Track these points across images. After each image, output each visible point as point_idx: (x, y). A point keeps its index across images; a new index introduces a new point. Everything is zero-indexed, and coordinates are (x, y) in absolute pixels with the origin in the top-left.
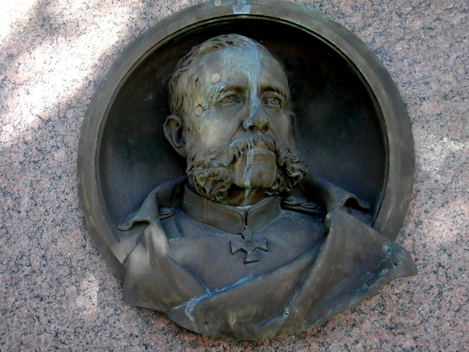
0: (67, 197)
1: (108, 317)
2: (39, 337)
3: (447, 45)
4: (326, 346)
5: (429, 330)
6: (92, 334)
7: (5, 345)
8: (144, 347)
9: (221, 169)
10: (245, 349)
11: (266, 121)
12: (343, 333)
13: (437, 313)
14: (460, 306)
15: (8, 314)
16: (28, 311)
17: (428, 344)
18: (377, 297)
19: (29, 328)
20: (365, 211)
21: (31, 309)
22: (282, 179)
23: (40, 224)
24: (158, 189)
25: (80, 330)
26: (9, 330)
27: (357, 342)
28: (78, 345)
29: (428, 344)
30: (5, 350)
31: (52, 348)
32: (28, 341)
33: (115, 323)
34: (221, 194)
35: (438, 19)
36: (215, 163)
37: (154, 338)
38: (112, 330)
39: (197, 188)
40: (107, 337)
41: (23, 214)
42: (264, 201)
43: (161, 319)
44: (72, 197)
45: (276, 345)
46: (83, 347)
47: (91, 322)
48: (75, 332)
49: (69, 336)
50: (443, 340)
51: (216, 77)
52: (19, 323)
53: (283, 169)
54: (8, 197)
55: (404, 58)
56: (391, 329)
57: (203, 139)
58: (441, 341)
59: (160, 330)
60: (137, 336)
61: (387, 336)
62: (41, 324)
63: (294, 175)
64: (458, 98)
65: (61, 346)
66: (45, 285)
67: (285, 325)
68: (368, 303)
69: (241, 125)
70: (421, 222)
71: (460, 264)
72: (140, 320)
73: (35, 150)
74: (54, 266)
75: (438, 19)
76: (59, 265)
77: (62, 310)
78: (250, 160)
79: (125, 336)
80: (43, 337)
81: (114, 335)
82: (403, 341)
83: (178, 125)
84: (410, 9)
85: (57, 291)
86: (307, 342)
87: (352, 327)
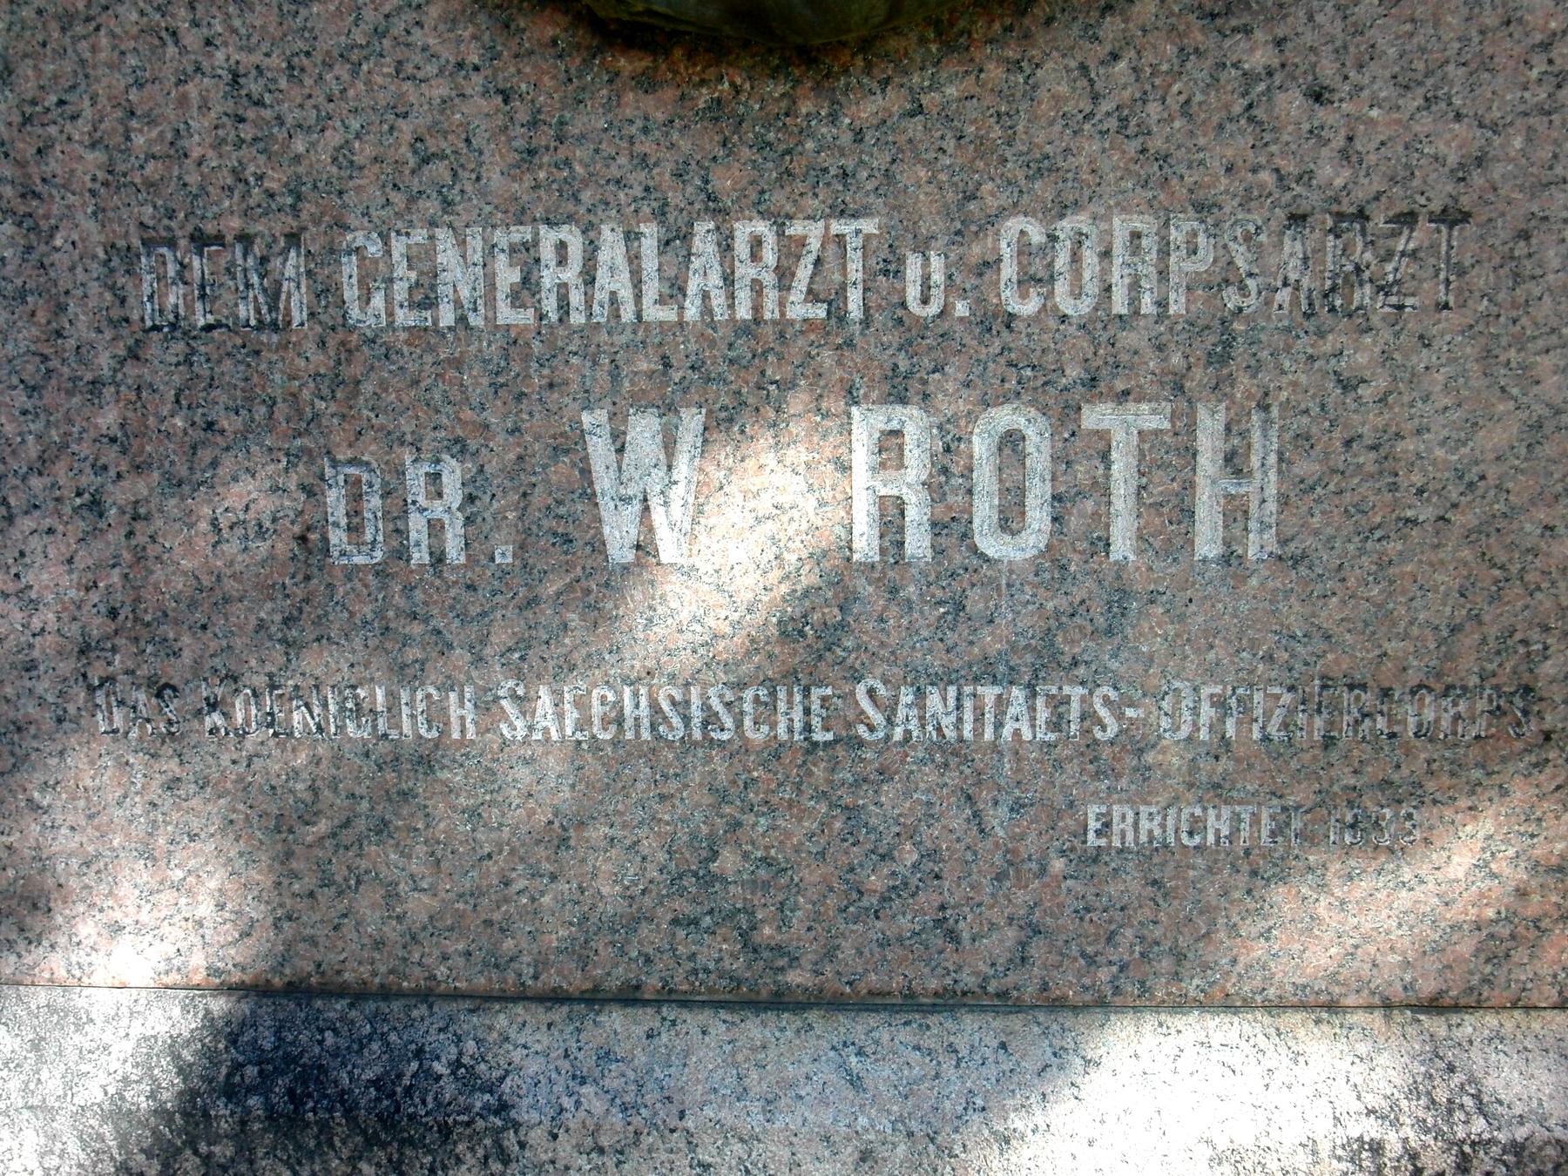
1: (387, 16)
2: (181, 89)
4: (1028, 72)
5: (1319, 18)
6: (342, 70)
7: (80, 121)
8: (500, 99)
10: (793, 88)
12: (1076, 30)
15: (79, 29)
16: (142, 13)
17: (1313, 59)
19: (148, 67)
21: (149, 9)
25: (305, 61)
26: (87, 76)
27: (1115, 57)
28: (301, 106)
29: (1313, 59)
30: (82, 133)
31: (225, 119)
32: (151, 104)
33: (408, 32)
37: (528, 70)
38: (400, 53)
40: (389, 75)
43: (547, 12)
45: (884, 71)
46: (318, 110)
47: (338, 34)
48: (291, 67)
49: (274, 81)
50: (1357, 46)
52: (116, 54)
56: (1213, 16)
58: (1352, 49)
59: (546, 45)
60: (476, 68)
61: (1200, 37)
62: (184, 50)
65: (251, 114)
72: (482, 18)
79: (441, 71)
80: (192, 89)
81: (409, 69)
82: (1244, 52)
86: (972, 60)
87: (1103, 16)
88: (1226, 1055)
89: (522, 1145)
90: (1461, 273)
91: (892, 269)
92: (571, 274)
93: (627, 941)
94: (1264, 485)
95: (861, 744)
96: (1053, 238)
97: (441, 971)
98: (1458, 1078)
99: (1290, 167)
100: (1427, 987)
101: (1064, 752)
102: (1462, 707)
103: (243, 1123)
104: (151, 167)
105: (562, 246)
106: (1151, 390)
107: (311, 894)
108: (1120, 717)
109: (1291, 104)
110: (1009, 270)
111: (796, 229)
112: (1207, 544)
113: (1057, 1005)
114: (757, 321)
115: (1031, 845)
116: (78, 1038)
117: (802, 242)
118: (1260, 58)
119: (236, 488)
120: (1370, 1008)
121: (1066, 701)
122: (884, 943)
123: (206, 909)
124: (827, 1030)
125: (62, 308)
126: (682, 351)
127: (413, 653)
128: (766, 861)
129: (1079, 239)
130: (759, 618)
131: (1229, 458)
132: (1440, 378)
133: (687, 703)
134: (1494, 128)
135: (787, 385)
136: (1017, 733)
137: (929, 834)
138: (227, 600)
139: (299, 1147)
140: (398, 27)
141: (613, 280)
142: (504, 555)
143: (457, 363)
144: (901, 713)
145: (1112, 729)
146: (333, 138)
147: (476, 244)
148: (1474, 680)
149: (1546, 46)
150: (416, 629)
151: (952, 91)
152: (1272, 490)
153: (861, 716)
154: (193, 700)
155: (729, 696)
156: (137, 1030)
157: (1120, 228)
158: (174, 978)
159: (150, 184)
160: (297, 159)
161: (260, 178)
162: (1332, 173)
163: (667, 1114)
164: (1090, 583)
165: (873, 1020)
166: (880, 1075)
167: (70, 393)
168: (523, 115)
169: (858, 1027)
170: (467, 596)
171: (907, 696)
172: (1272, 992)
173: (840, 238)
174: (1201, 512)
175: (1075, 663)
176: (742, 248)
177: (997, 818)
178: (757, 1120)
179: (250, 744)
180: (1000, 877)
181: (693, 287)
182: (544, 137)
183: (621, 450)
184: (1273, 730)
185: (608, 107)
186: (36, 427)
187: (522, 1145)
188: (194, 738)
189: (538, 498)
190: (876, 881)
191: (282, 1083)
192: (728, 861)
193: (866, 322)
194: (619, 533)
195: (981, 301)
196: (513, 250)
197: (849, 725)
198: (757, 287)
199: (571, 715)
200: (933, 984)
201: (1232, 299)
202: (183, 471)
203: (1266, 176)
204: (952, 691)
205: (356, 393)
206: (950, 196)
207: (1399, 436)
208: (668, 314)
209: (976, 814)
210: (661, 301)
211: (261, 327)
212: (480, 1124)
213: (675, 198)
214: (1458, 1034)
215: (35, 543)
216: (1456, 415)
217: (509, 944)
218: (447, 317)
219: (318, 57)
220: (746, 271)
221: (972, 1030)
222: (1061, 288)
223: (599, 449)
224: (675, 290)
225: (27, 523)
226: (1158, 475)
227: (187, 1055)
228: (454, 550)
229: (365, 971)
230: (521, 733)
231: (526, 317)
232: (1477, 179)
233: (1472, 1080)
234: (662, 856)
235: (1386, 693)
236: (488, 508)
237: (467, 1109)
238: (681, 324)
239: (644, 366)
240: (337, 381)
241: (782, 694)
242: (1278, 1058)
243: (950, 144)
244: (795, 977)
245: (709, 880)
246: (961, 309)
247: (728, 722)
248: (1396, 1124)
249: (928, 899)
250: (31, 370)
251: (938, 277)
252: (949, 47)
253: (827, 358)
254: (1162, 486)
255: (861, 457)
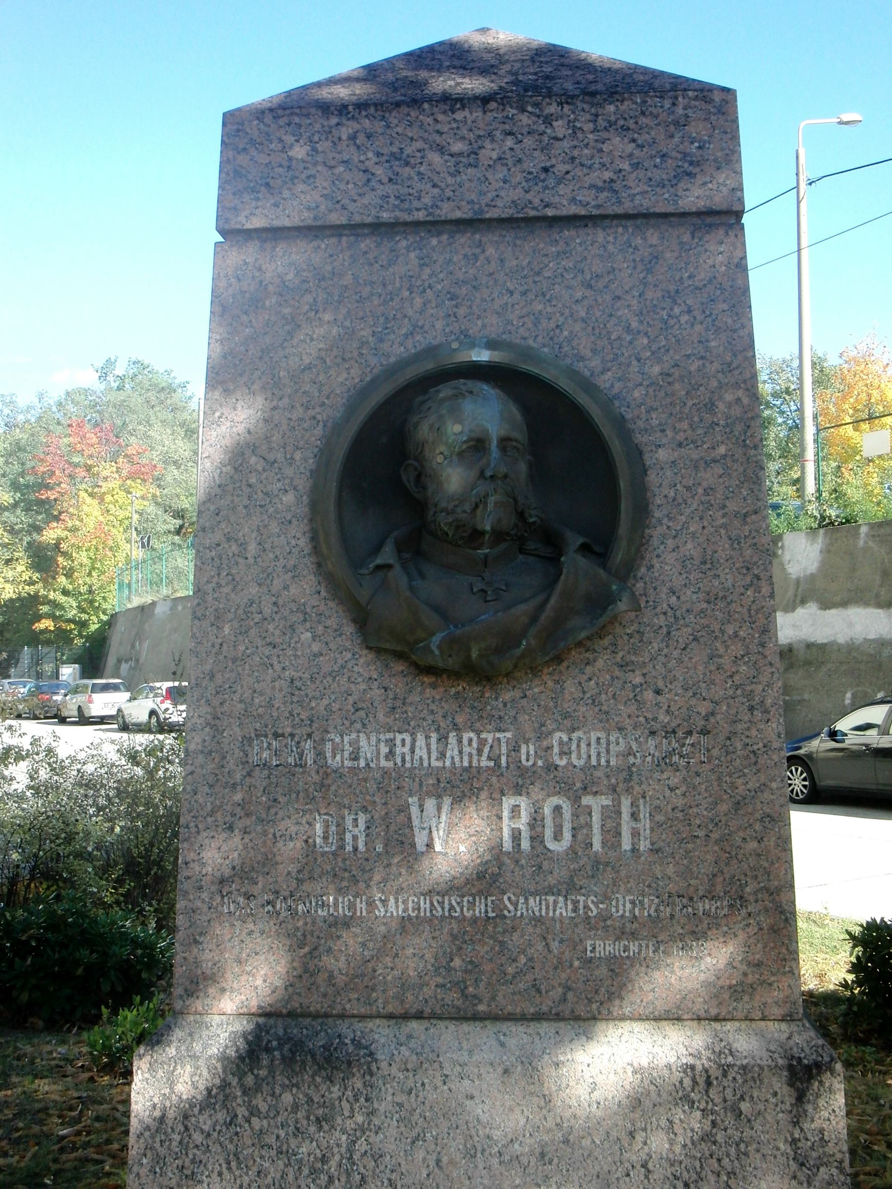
0: (299, 542)
3: (683, 393)
6: (330, 679)
9: (465, 515)
11: (505, 470)
12: (577, 670)
13: (665, 651)
14: (687, 645)
15: (239, 663)
18: (610, 637)
20: (599, 555)
22: (520, 524)
23: (270, 570)
24: (395, 533)
27: (590, 679)
34: (462, 538)
35: (676, 365)
36: (459, 510)
38: (350, 674)
39: (439, 533)
41: (251, 561)
42: (503, 546)
44: (303, 542)
51: (457, 428)
53: (521, 515)
54: (232, 543)
55: (642, 404)
57: (446, 485)
62: (275, 671)
63: (532, 520)
64: (692, 446)
65: (297, 693)
66: (277, 632)
67: (523, 656)
68: (601, 642)
69: (482, 474)
70: (652, 566)
71: (688, 606)
72: (378, 663)
73: (260, 493)
74: (286, 613)
75: (676, 365)
76: (292, 612)
77: (295, 656)
78: (490, 506)
80: (277, 684)
83: (416, 469)
84: (649, 354)
85: (291, 638)
88: (639, 1036)
89: (378, 1068)
90: (708, 751)
91: (516, 749)
92: (406, 750)
93: (419, 993)
94: (645, 824)
95: (505, 917)
96: (570, 739)
97: (348, 1007)
98: (723, 1044)
99: (649, 716)
100: (714, 1012)
101: (577, 920)
102: (719, 904)
103: (272, 1061)
104: (260, 710)
105: (403, 740)
106: (605, 791)
107: (300, 976)
108: (597, 907)
109: (649, 695)
110: (556, 750)
111: (484, 735)
112: (626, 845)
113: (578, 1018)
114: (470, 767)
115: (567, 956)
116: (207, 1032)
117: (486, 740)
118: (638, 680)
119: (283, 823)
120: (692, 1020)
121: (578, 901)
122: (514, 994)
123: (259, 982)
124: (491, 1028)
125: (225, 758)
126: (445, 776)
127: (345, 883)
128: (471, 962)
129: (579, 740)
130: (469, 871)
131: (633, 815)
132: (703, 787)
133: (443, 902)
134: (716, 703)
135: (480, 789)
136: (561, 914)
137: (530, 952)
138: (277, 863)
139: (293, 1071)
140: (349, 665)
141: (421, 751)
142: (379, 848)
143: (365, 780)
144: (520, 906)
145: (595, 912)
146: (325, 702)
147: (373, 739)
148: (722, 894)
149: (731, 676)
150: (346, 875)
151: (536, 690)
152: (648, 826)
153: (505, 907)
154: (260, 901)
155: (459, 900)
156: (230, 1029)
157: (593, 736)
158: (245, 1010)
159: (259, 716)
160: (312, 709)
161: (299, 714)
162: (664, 718)
163: (432, 1056)
164: (585, 859)
165: (509, 1024)
166: (512, 1042)
167: (225, 788)
168: (391, 696)
169: (505, 1026)
170: (365, 863)
171: (522, 900)
172: (656, 1013)
173: (499, 739)
174: (624, 834)
175: (581, 888)
176: (465, 741)
177: (555, 945)
178: (465, 1058)
179: (281, 918)
180: (556, 968)
181: (448, 755)
182: (398, 703)
183: (422, 811)
184: (652, 912)
185: (420, 693)
186: (212, 799)
187: (378, 1068)
188: (260, 915)
189: (392, 828)
190: (510, 970)
191: (287, 1047)
192: (457, 963)
193: (508, 767)
194: (420, 840)
195: (546, 760)
196: (387, 741)
197: (501, 910)
198: (470, 755)
199: (401, 907)
200: (532, 1010)
201: (632, 760)
202: (264, 816)
203: (641, 719)
204: (538, 898)
205: (328, 790)
206: (536, 725)
207: (690, 807)
208: (439, 764)
209: (547, 944)
210: (437, 759)
211: (296, 765)
212: (363, 1060)
213: (443, 725)
214: (725, 1029)
215: (207, 841)
216: (710, 800)
217: (374, 995)
218: (362, 764)
219: (321, 674)
220: (467, 750)
221: (545, 1027)
222: (574, 756)
223: (414, 810)
224: (442, 755)
225: (205, 834)
226: (608, 820)
227: (250, 1038)
228: (361, 847)
229: (319, 1006)
230: (382, 914)
231: (390, 764)
232: (712, 720)
233: (729, 1044)
234: (433, 961)
235: (691, 899)
236: (374, 831)
237: (357, 1055)
238: (444, 767)
239: (431, 782)
240: (322, 785)
241: (477, 899)
242: (658, 1038)
243: (536, 708)
244: (481, 1008)
245: (449, 969)
246: (540, 763)
247: (458, 909)
248: (700, 1058)
249: (529, 977)
250: (211, 779)
251: (532, 752)
252: (535, 675)
253: (494, 779)
254: (610, 824)
255: (506, 814)
